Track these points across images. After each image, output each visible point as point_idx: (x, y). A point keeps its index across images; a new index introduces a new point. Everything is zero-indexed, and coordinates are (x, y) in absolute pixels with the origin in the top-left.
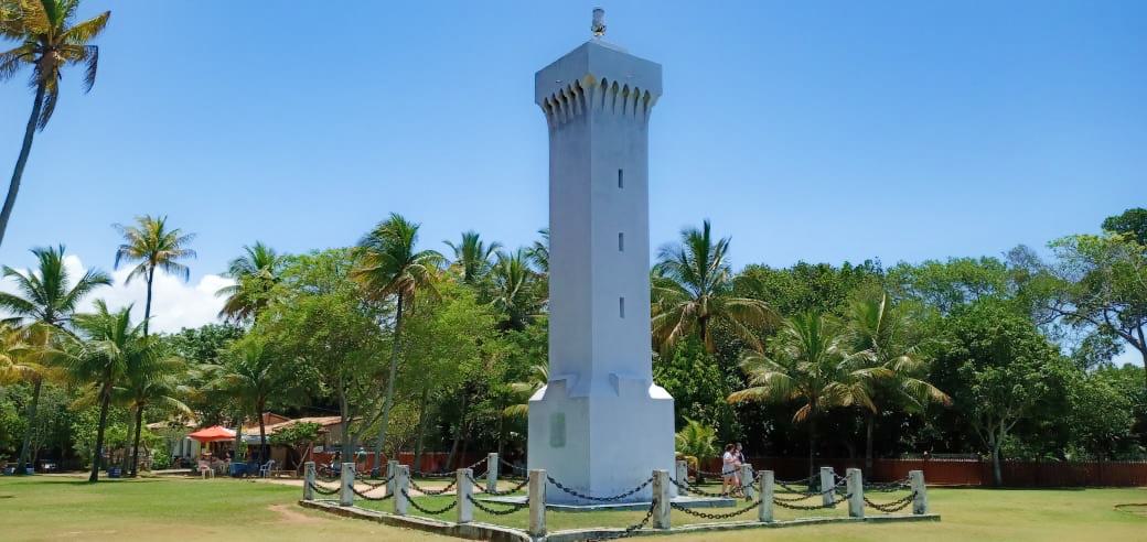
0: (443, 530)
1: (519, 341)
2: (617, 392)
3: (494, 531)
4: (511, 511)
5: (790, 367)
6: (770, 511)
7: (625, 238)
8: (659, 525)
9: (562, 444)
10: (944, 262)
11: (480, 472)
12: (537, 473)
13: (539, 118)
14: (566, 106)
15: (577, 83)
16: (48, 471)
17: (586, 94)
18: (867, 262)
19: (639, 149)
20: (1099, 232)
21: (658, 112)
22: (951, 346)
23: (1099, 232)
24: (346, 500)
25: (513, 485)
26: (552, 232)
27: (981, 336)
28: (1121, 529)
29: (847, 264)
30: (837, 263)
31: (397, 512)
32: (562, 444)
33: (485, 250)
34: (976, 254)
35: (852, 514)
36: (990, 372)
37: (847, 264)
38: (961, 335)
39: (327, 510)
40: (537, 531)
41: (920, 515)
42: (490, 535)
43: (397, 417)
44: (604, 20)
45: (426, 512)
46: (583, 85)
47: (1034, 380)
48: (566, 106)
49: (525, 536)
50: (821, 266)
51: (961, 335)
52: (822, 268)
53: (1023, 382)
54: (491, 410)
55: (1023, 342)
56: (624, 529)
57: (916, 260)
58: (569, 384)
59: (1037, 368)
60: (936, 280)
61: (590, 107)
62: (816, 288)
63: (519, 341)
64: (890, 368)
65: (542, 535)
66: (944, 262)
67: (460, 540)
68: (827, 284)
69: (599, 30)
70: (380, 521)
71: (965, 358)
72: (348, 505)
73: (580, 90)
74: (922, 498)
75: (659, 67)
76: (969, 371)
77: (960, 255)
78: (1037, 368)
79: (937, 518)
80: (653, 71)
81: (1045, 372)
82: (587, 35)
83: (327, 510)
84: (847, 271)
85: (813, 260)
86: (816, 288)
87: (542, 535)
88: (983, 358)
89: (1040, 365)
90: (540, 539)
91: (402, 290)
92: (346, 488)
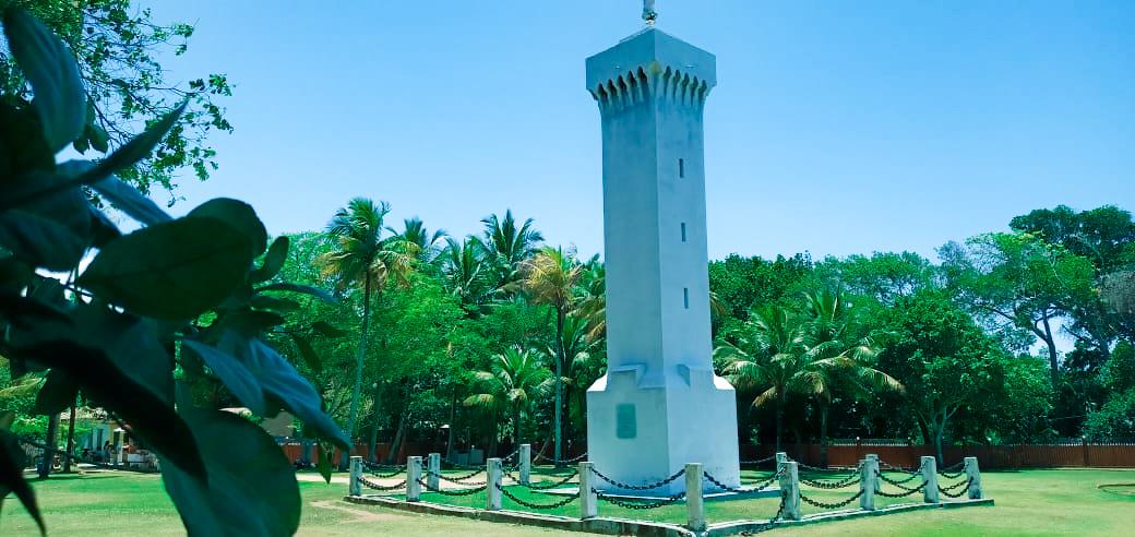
0: (567, 526)
1: (478, 330)
2: (688, 383)
3: (641, 526)
4: (562, 503)
5: (762, 358)
6: (872, 500)
7: (686, 226)
8: (790, 516)
9: (632, 435)
10: (869, 256)
11: (515, 464)
12: (696, 466)
13: (592, 108)
14: (634, 92)
15: (641, 70)
16: (127, 467)
17: (650, 81)
18: (797, 256)
19: (694, 139)
20: (1008, 231)
21: (709, 100)
22: (903, 338)
23: (1008, 231)
24: (414, 496)
25: (908, 476)
26: (127, 236)
27: (927, 328)
28: (1118, 516)
29: (780, 257)
30: (770, 256)
31: (493, 507)
32: (632, 435)
33: (429, 238)
34: (898, 250)
35: (927, 500)
36: (939, 362)
37: (780, 257)
38: (908, 326)
39: (393, 506)
40: (697, 525)
41: (977, 500)
42: (636, 530)
43: (351, 405)
44: (656, 8)
45: (827, 506)
46: (648, 72)
47: (978, 368)
48: (634, 92)
49: (685, 531)
50: (755, 258)
51: (908, 326)
52: (756, 261)
53: (969, 370)
54: (433, 399)
55: (966, 333)
56: (768, 521)
57: (842, 255)
58: (639, 374)
59: (979, 357)
60: (864, 274)
61: (643, 94)
62: (752, 280)
63: (478, 330)
64: (850, 356)
65: (703, 530)
66: (869, 256)
67: (596, 535)
68: (762, 276)
69: (652, 18)
70: (473, 517)
71: (913, 348)
72: (416, 500)
73: (642, 76)
74: (977, 484)
75: (714, 57)
76: (918, 360)
77: (885, 251)
78: (979, 357)
79: (991, 502)
80: (708, 60)
81: (987, 362)
82: (638, 26)
83: (393, 506)
84: (780, 264)
85: (746, 254)
86: (752, 280)
87: (703, 530)
88: (932, 349)
89: (982, 355)
90: (703, 534)
91: (371, 277)
92: (493, 487)
